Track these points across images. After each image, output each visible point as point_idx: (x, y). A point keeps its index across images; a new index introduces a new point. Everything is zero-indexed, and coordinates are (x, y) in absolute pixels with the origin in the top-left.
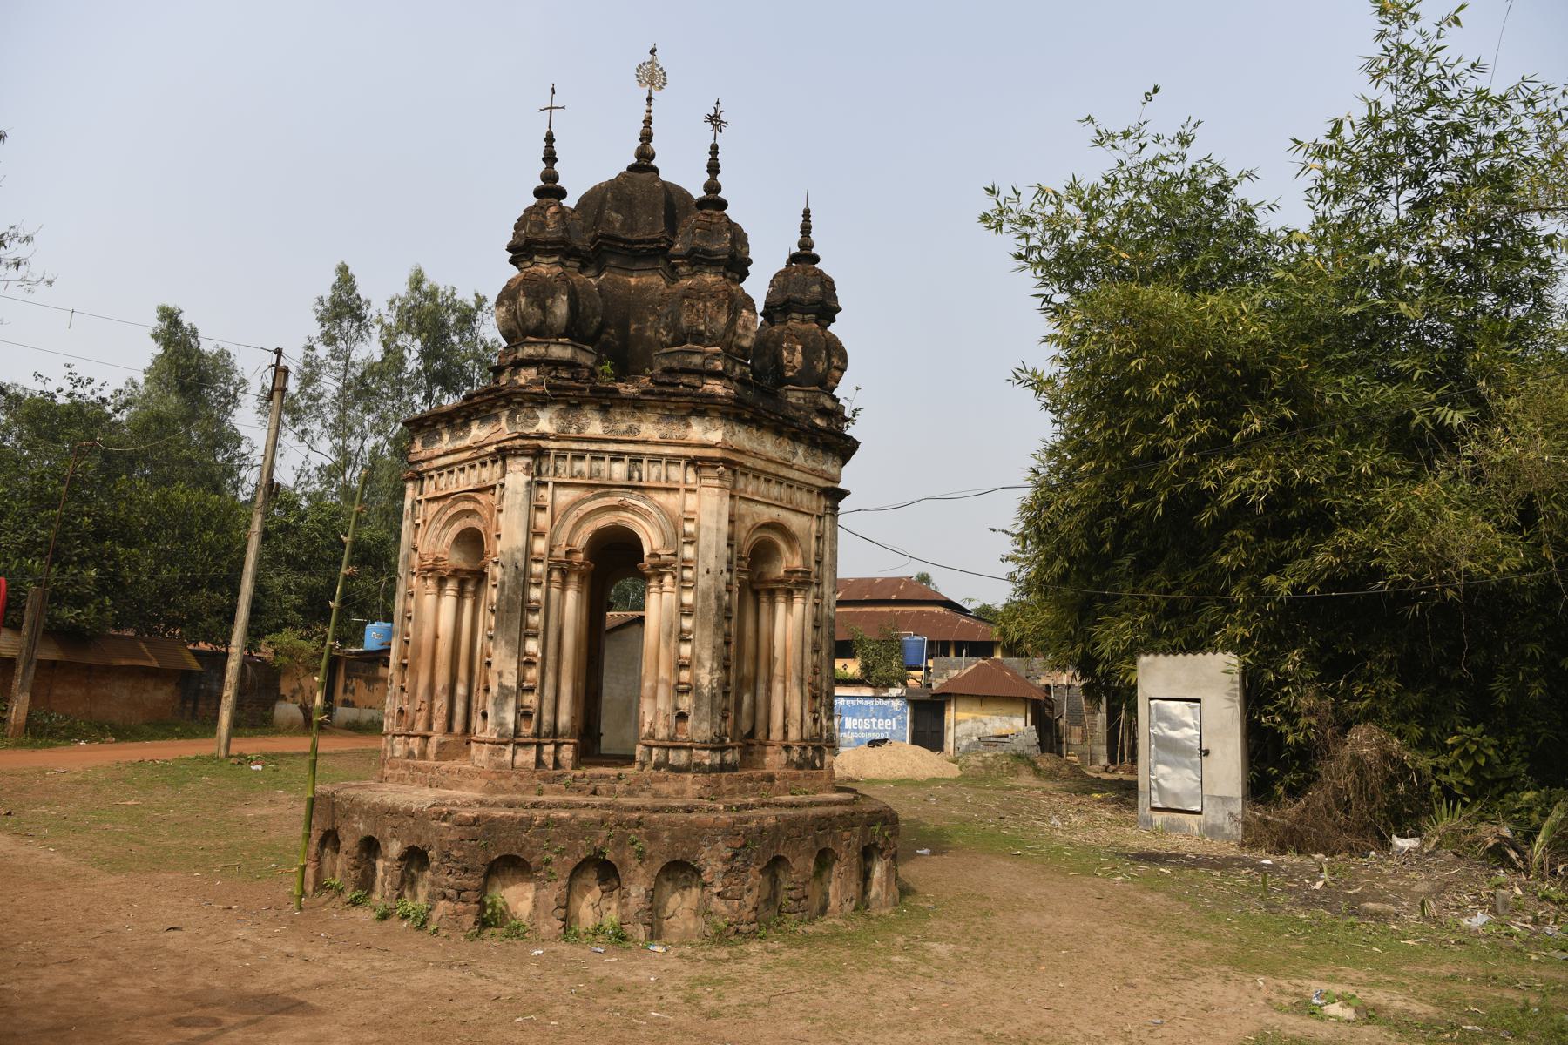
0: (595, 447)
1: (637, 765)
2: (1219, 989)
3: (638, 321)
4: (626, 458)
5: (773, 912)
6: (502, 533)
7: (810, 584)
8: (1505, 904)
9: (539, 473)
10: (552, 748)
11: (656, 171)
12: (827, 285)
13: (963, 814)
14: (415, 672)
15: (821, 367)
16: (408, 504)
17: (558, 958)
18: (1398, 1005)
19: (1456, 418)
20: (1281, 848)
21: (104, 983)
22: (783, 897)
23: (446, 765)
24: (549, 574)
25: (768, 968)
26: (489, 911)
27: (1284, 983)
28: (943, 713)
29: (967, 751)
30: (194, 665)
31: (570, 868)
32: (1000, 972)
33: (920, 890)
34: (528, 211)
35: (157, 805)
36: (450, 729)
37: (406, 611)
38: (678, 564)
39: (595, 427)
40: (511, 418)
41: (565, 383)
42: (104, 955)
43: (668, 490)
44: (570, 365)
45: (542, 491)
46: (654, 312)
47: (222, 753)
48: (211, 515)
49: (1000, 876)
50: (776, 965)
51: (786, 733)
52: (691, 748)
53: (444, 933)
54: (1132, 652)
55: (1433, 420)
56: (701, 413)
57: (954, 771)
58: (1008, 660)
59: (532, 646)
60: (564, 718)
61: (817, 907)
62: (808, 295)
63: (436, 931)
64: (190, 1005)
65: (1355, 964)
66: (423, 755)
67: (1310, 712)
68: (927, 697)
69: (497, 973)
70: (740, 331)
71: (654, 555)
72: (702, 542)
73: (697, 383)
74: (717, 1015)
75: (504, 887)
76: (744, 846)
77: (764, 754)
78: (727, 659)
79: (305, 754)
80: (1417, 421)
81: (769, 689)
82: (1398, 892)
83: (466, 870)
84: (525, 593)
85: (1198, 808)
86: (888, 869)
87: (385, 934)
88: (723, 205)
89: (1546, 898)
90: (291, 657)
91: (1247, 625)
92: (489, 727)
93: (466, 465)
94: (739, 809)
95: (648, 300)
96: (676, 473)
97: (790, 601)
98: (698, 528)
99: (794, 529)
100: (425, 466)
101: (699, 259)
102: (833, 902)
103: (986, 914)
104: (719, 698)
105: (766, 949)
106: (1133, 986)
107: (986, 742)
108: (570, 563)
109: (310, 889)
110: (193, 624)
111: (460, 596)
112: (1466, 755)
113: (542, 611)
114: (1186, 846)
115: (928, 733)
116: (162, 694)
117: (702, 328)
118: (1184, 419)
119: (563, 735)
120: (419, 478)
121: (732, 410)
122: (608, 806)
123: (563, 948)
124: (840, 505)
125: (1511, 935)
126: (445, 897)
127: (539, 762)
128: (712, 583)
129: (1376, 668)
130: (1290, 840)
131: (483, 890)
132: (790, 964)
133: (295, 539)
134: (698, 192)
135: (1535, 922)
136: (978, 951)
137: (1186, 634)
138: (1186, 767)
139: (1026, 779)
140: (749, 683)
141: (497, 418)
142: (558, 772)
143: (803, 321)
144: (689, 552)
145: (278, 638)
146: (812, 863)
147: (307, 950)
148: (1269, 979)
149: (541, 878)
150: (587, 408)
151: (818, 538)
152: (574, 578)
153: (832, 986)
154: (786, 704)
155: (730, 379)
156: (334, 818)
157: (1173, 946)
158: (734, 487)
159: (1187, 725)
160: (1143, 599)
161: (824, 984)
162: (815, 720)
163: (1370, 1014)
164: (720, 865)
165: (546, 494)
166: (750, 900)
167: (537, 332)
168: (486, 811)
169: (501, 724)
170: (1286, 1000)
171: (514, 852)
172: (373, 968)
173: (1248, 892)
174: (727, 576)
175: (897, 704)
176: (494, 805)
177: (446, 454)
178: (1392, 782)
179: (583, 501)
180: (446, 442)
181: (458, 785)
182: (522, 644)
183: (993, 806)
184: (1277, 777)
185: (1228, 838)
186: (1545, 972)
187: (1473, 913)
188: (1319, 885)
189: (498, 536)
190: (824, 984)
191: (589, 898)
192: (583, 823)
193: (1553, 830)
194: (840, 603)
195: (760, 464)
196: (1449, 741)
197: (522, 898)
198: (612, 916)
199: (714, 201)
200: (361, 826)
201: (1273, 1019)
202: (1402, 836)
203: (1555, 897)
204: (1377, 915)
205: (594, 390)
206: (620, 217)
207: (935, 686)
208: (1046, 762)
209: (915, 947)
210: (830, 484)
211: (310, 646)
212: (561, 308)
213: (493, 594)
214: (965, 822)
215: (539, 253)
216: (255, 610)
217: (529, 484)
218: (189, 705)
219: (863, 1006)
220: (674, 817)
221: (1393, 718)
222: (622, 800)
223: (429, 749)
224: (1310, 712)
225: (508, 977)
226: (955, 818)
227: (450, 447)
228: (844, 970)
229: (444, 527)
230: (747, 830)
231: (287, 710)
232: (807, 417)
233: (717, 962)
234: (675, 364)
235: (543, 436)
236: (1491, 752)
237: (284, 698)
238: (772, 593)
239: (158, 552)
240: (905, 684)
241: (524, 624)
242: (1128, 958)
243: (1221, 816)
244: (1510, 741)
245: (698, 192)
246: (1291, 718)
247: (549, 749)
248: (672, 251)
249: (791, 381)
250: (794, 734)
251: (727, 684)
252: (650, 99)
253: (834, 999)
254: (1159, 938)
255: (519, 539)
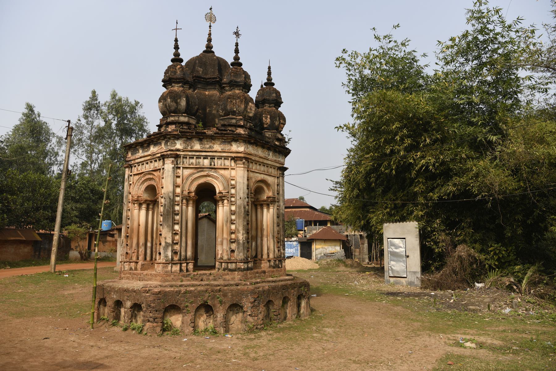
0: (197, 154)
1: (217, 270)
2: (428, 339)
3: (209, 108)
4: (209, 158)
5: (268, 321)
6: (164, 186)
7: (275, 201)
8: (516, 305)
9: (177, 164)
10: (185, 264)
11: (213, 52)
12: (278, 94)
13: (324, 281)
14: (132, 239)
15: (277, 123)
16: (126, 176)
17: (194, 342)
18: (489, 341)
19: (494, 138)
20: (435, 289)
21: (24, 361)
22: (272, 315)
23: (145, 272)
24: (182, 201)
25: (270, 341)
26: (166, 325)
27: (449, 336)
28: (311, 246)
29: (320, 259)
30: (39, 238)
31: (195, 308)
32: (352, 337)
33: (317, 309)
34: (170, 67)
35: (30, 291)
36: (145, 259)
37: (127, 216)
38: (229, 196)
39: (197, 146)
40: (166, 144)
41: (186, 130)
42: (21, 350)
43: (225, 169)
44: (187, 124)
45: (178, 170)
46: (216, 104)
47: (53, 271)
48: (43, 182)
49: (343, 303)
50: (273, 339)
51: (268, 256)
52: (236, 262)
53: (149, 334)
54: (382, 222)
55: (485, 139)
56: (236, 141)
57: (317, 266)
58: (333, 227)
59: (177, 227)
60: (189, 254)
61: (283, 318)
62: (271, 97)
63: (146, 334)
64: (58, 367)
65: (470, 328)
66: (136, 269)
67: (443, 241)
68: (305, 240)
69: (171, 350)
70: (249, 110)
71: (220, 193)
72: (238, 188)
73: (234, 130)
74: (257, 359)
75: (171, 316)
76: (258, 297)
77: (261, 263)
78: (248, 230)
79: (92, 269)
80: (479, 139)
81: (262, 240)
82: (479, 302)
83: (157, 311)
84: (173, 208)
85: (405, 276)
86: (307, 303)
87: (127, 336)
88: (241, 64)
89: (529, 302)
90: (75, 234)
91: (422, 211)
92: (162, 258)
93: (149, 161)
94: (255, 283)
95: (214, 99)
96: (227, 163)
97: (268, 208)
98: (236, 182)
99: (269, 182)
100: (133, 162)
101: (233, 84)
102: (289, 316)
103: (342, 317)
104: (246, 244)
105: (267, 334)
106: (398, 340)
107: (327, 255)
108: (189, 196)
109: (95, 320)
110: (37, 223)
111: (147, 210)
112: (495, 254)
113: (180, 215)
114: (402, 289)
115: (306, 253)
116: (26, 250)
117: (235, 109)
118: (402, 140)
119: (189, 260)
120: (130, 167)
121: (247, 139)
122: (208, 285)
123: (194, 337)
124: (285, 173)
125: (519, 315)
126: (149, 321)
127: (181, 270)
128: (242, 202)
129: (465, 225)
130: (438, 286)
131: (163, 318)
132: (277, 339)
133: (74, 191)
134: (230, 60)
135: (526, 310)
136: (342, 331)
137: (400, 215)
138: (401, 262)
139: (342, 268)
140: (255, 238)
141: (160, 144)
142: (188, 273)
143: (270, 107)
144: (233, 191)
145: (70, 227)
146: (281, 302)
147: (99, 344)
148: (444, 335)
149: (184, 313)
150: (194, 139)
151: (278, 185)
152: (191, 202)
153: (295, 346)
154: (268, 245)
155: (246, 128)
156: (104, 294)
157: (408, 325)
158: (248, 167)
159: (401, 247)
160: (385, 203)
161: (292, 346)
162: (279, 251)
163: (481, 345)
164: (250, 304)
165: (180, 171)
166: (261, 316)
167: (175, 112)
168: (163, 289)
169: (166, 256)
170: (451, 342)
171: (174, 303)
172: (125, 349)
173: (429, 304)
174: (247, 199)
175: (295, 243)
176: (166, 286)
177: (141, 158)
178: (471, 264)
179: (194, 174)
180: (140, 153)
181: (150, 280)
182: (173, 227)
183: (334, 278)
184: (432, 264)
185: (416, 286)
186: (534, 327)
187: (505, 308)
188: (452, 301)
189: (163, 187)
190: (292, 346)
191: (202, 319)
192: (199, 292)
193: (528, 278)
194: (286, 208)
195: (257, 159)
196: (490, 249)
197: (177, 320)
198: (211, 325)
199: (237, 63)
200: (115, 296)
201: (449, 349)
202: (478, 283)
203: (532, 301)
204: (473, 311)
205: (197, 133)
206: (201, 69)
207: (308, 236)
208: (349, 262)
209: (320, 330)
210: (281, 166)
211: (82, 230)
212: (183, 103)
213: (161, 209)
214: (325, 284)
215: (174, 82)
216: (63, 218)
217: (173, 168)
218: (37, 253)
219: (308, 353)
220: (232, 288)
221: (471, 242)
222: (212, 282)
223: (138, 267)
224: (443, 241)
225: (176, 350)
226: (322, 283)
227: (142, 155)
228: (297, 340)
229: (141, 184)
230: (259, 291)
231: (74, 254)
232: (273, 141)
233: (251, 339)
234: (226, 123)
235: (178, 150)
236: (504, 253)
237: (72, 249)
238: (262, 206)
239: (23, 197)
240: (297, 236)
241: (174, 219)
242: (394, 330)
243: (413, 278)
244: (510, 249)
245: (230, 60)
246: (436, 243)
247: (184, 265)
248: (223, 81)
249: (266, 128)
250: (271, 256)
251: (248, 238)
252: (210, 26)
253: (297, 351)
254: (403, 322)
255: (171, 188)
